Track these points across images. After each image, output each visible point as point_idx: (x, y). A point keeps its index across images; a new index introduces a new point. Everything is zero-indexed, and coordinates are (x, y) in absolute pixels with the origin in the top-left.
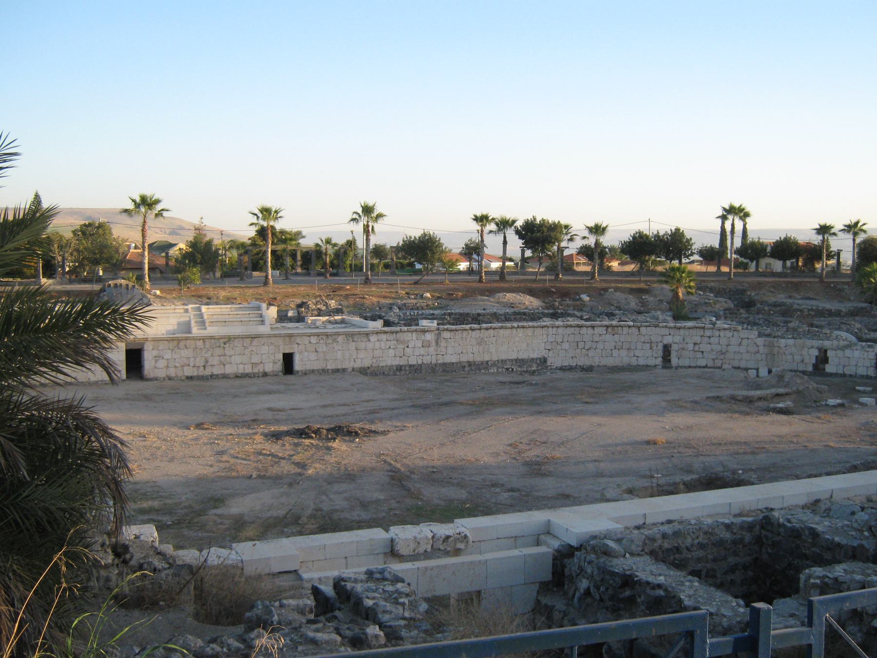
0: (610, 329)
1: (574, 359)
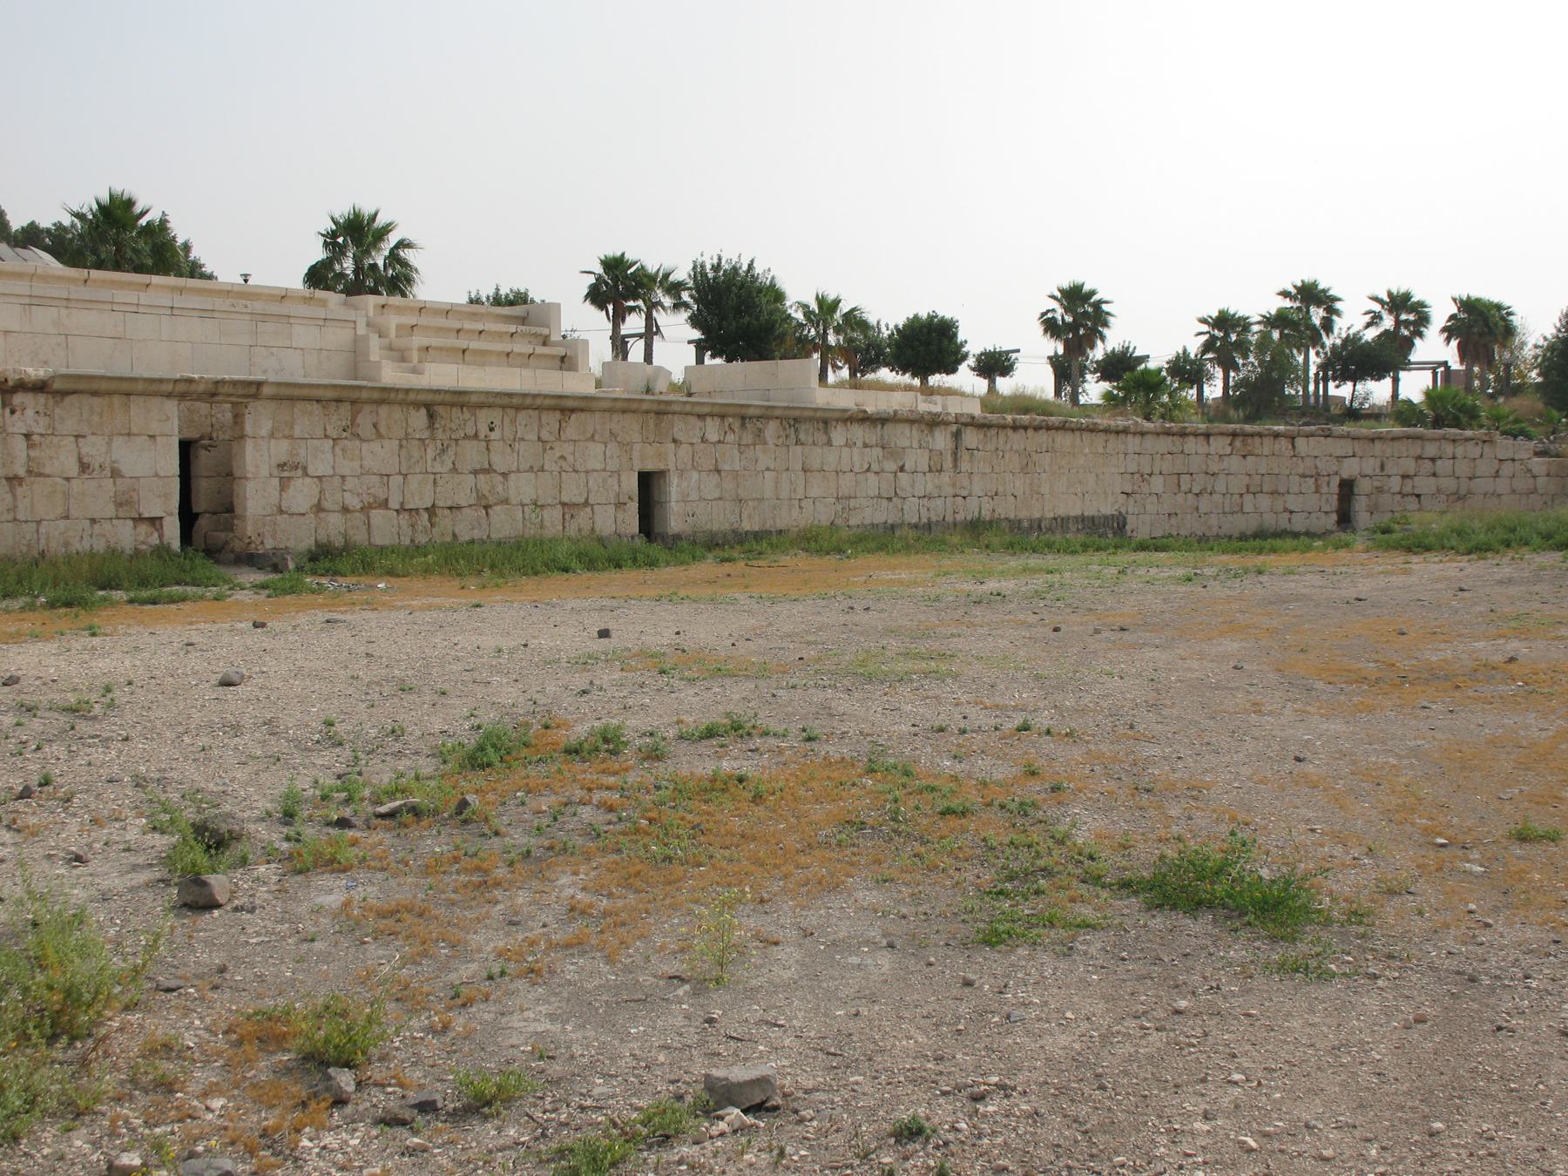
0: (1238, 443)
1: (1173, 521)
